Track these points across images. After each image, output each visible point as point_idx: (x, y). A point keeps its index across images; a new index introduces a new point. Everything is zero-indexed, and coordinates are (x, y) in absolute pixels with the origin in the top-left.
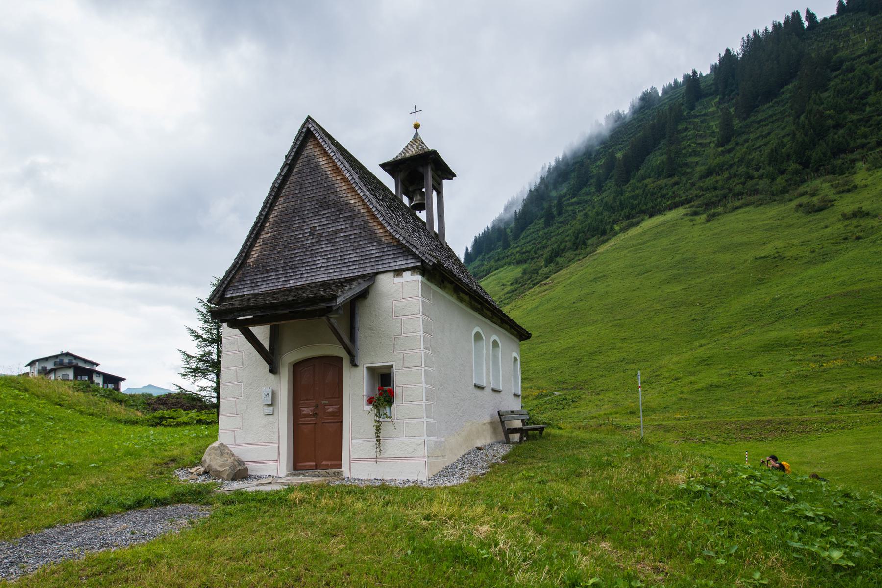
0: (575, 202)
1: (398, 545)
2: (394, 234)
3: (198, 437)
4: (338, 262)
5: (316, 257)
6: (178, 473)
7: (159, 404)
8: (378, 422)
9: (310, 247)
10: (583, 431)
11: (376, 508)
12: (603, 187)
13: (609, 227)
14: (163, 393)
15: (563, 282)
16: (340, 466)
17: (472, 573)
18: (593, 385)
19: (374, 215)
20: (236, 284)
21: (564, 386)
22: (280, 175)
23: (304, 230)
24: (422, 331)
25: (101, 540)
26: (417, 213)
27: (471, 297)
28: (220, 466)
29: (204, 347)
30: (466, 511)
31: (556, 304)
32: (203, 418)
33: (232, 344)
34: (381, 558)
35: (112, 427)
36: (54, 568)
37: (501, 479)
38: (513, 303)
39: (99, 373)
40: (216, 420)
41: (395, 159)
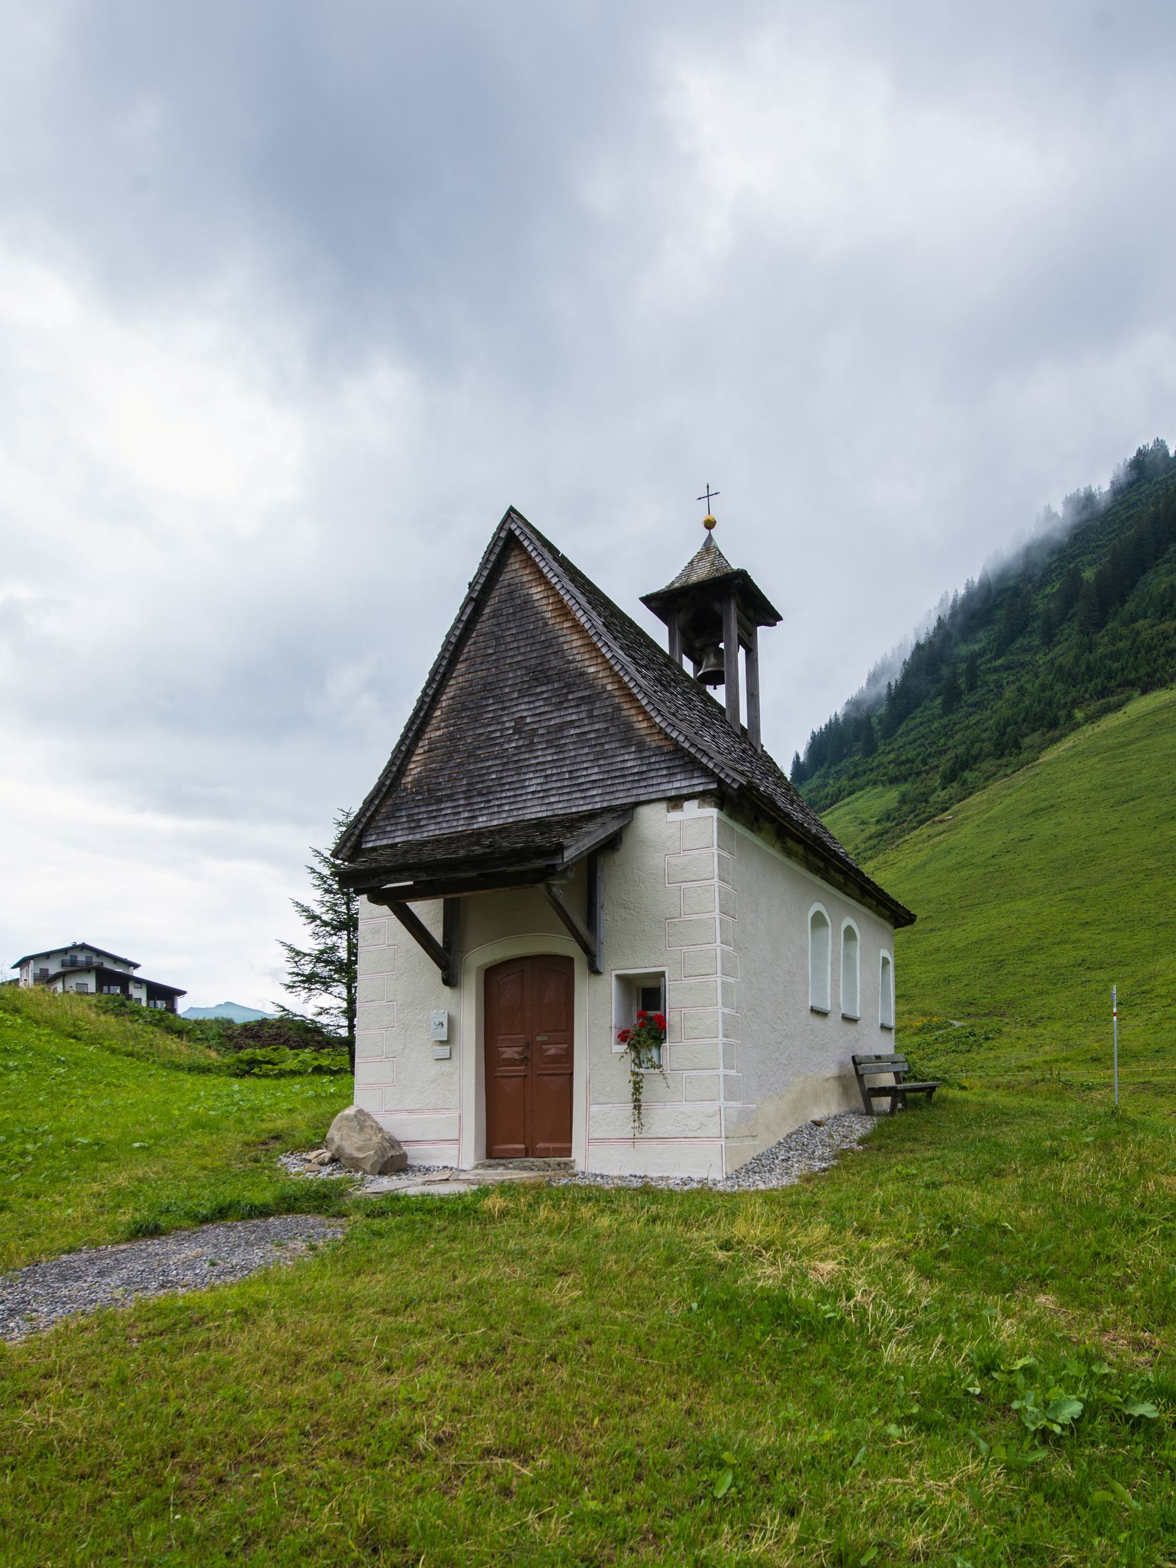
0: (1002, 666)
1: (675, 1293)
2: (668, 730)
3: (317, 1096)
4: (566, 783)
5: (525, 773)
6: (285, 1160)
7: (247, 1037)
8: (637, 1074)
9: (514, 755)
10: (1004, 1093)
11: (635, 1227)
12: (1055, 636)
13: (1064, 713)
14: (253, 1018)
15: (975, 818)
16: (568, 1151)
17: (805, 1345)
18: (1024, 1009)
19: (631, 695)
20: (382, 824)
21: (972, 1010)
22: (458, 620)
23: (504, 722)
24: (717, 911)
25: (159, 1276)
26: (709, 689)
27: (807, 847)
28: (359, 1149)
29: (324, 936)
30: (795, 1236)
31: (959, 859)
32: (325, 1062)
33: (376, 932)
34: (645, 1315)
35: (167, 1076)
36: (83, 1321)
37: (857, 1179)
38: (881, 858)
39: (139, 982)
40: (347, 1067)
41: (669, 587)
